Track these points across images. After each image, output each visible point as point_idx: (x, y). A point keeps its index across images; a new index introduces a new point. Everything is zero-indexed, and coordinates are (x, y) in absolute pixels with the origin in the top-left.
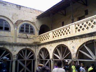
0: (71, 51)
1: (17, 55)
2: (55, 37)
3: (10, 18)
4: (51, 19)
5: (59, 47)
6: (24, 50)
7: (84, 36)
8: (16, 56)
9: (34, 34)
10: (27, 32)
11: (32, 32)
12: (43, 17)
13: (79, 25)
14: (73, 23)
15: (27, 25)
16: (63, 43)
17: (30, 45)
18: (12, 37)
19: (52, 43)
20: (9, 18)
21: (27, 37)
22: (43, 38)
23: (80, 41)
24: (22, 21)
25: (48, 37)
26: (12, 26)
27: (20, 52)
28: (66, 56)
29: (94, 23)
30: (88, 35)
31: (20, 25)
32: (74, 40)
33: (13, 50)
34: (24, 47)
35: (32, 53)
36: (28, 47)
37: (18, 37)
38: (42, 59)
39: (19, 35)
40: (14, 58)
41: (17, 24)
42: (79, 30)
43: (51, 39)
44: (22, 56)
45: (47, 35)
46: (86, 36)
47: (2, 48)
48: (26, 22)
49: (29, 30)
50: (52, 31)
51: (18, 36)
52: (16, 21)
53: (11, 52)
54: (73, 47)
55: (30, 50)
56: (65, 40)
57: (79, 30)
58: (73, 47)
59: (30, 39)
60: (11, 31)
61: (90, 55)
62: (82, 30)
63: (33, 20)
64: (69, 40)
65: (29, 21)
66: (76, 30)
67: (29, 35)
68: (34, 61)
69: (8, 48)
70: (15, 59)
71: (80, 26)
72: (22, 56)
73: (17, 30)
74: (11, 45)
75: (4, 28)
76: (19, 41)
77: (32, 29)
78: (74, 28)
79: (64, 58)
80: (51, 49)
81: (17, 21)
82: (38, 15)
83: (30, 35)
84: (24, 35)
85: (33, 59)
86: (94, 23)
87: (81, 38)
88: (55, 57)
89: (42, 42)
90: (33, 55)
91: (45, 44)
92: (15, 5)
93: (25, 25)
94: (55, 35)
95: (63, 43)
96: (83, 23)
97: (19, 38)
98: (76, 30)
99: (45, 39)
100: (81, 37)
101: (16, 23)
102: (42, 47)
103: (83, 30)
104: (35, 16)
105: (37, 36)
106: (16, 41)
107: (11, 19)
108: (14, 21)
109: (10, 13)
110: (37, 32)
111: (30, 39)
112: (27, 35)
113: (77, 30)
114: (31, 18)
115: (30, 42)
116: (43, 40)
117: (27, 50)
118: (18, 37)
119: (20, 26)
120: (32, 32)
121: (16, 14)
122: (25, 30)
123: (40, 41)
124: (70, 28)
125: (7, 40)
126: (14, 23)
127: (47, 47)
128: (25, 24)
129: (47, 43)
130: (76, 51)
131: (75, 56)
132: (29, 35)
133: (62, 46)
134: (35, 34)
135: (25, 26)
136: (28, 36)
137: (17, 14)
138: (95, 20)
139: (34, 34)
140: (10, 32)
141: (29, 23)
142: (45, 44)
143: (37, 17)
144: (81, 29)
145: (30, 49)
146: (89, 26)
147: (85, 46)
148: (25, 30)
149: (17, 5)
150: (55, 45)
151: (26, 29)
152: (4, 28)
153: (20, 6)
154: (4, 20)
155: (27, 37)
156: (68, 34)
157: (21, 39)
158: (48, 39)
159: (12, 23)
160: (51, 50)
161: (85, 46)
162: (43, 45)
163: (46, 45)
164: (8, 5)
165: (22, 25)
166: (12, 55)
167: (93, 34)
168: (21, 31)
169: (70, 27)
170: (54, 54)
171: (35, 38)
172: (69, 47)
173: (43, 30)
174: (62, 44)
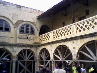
0: (72, 52)
1: (17, 55)
2: (55, 38)
3: (10, 18)
4: (52, 19)
5: (59, 48)
6: (24, 51)
7: (85, 37)
8: (16, 57)
9: (35, 35)
10: (27, 32)
11: (33, 32)
12: (43, 17)
13: (79, 26)
14: (74, 24)
15: (28, 26)
16: (63, 43)
17: (31, 46)
18: (13, 38)
19: (52, 44)
20: (9, 18)
21: (28, 37)
22: (43, 38)
23: (81, 42)
24: (23, 21)
25: (49, 37)
26: (12, 26)
27: (21, 52)
28: (67, 57)
29: (95, 23)
30: (89, 36)
31: (20, 26)
32: (75, 40)
33: (13, 51)
34: (24, 48)
35: (32, 54)
36: (28, 48)
37: (18, 38)
38: (43, 60)
39: (19, 36)
40: (15, 59)
41: (17, 24)
42: (80, 31)
43: (52, 40)
44: (23, 57)
45: (48, 36)
46: (87, 36)
47: (2, 48)
48: (26, 23)
49: (30, 31)
50: (52, 31)
51: (18, 37)
52: (16, 21)
53: (11, 53)
54: (74, 48)
55: (30, 50)
56: (66, 40)
57: (80, 31)
58: (74, 48)
59: (30, 40)
60: (11, 31)
61: (91, 56)
62: (83, 30)
63: (33, 20)
64: (70, 40)
65: (29, 22)
66: (77, 30)
67: (29, 36)
68: (34, 62)
69: (8, 48)
70: (15, 59)
71: (80, 27)
72: (23, 57)
73: (17, 31)
74: (11, 45)
75: (4, 29)
76: (19, 41)
77: (32, 29)
78: (75, 28)
79: (65, 59)
80: (51, 49)
81: (17, 22)
82: (38, 15)
83: (30, 35)
84: (24, 36)
85: (33, 60)
86: (95, 23)
87: (82, 38)
88: (55, 58)
89: (43, 43)
90: (33, 55)
91: (46, 44)
92: (16, 6)
93: (25, 26)
94: (55, 35)
95: (63, 43)
96: (84, 24)
97: (19, 39)
98: (77, 30)
99: (46, 39)
100: (82, 37)
101: (16, 24)
102: (43, 47)
103: (84, 31)
104: (36, 16)
105: (38, 36)
106: (16, 42)
107: (11, 19)
108: (15, 22)
109: (10, 14)
110: (37, 33)
111: (30, 39)
112: (28, 35)
113: (78, 31)
114: (32, 18)
115: (30, 42)
116: (43, 41)
117: (27, 50)
118: (18, 38)
119: (20, 26)
120: (33, 32)
121: (16, 14)
122: (25, 30)
123: (41, 42)
124: (70, 28)
125: (7, 41)
126: (14, 23)
127: (48, 48)
128: (25, 24)
129: (48, 44)
130: (77, 51)
131: (76, 57)
132: (30, 35)
133: (63, 47)
134: (36, 35)
135: (25, 27)
136: (28, 36)
137: (17, 14)
138: (96, 21)
139: (35, 35)
140: (10, 32)
141: (29, 23)
142: (46, 44)
143: (37, 17)
144: (82, 30)
145: (31, 50)
146: (90, 27)
147: (86, 47)
148: (25, 30)
149: (17, 5)
150: (55, 46)
151: (26, 29)
152: (4, 29)
153: (20, 6)
154: (4, 21)
155: (28, 37)
156: (69, 34)
157: (21, 39)
158: (49, 39)
159: (13, 23)
160: (51, 50)
161: (86, 47)
162: (44, 45)
163: (47, 46)
164: (8, 5)
165: (23, 25)
166: (12, 56)
167: (94, 35)
168: (22, 31)
169: (71, 27)
170: (55, 55)
171: (35, 38)
172: (70, 48)
173: (44, 30)
174: (62, 45)
